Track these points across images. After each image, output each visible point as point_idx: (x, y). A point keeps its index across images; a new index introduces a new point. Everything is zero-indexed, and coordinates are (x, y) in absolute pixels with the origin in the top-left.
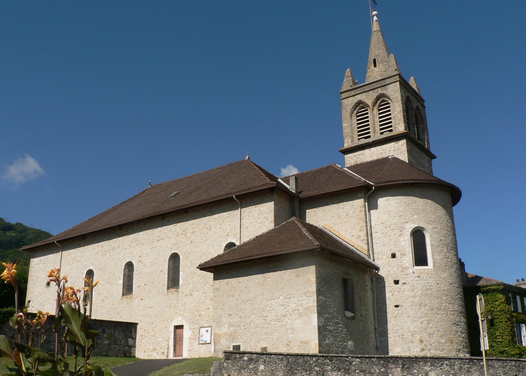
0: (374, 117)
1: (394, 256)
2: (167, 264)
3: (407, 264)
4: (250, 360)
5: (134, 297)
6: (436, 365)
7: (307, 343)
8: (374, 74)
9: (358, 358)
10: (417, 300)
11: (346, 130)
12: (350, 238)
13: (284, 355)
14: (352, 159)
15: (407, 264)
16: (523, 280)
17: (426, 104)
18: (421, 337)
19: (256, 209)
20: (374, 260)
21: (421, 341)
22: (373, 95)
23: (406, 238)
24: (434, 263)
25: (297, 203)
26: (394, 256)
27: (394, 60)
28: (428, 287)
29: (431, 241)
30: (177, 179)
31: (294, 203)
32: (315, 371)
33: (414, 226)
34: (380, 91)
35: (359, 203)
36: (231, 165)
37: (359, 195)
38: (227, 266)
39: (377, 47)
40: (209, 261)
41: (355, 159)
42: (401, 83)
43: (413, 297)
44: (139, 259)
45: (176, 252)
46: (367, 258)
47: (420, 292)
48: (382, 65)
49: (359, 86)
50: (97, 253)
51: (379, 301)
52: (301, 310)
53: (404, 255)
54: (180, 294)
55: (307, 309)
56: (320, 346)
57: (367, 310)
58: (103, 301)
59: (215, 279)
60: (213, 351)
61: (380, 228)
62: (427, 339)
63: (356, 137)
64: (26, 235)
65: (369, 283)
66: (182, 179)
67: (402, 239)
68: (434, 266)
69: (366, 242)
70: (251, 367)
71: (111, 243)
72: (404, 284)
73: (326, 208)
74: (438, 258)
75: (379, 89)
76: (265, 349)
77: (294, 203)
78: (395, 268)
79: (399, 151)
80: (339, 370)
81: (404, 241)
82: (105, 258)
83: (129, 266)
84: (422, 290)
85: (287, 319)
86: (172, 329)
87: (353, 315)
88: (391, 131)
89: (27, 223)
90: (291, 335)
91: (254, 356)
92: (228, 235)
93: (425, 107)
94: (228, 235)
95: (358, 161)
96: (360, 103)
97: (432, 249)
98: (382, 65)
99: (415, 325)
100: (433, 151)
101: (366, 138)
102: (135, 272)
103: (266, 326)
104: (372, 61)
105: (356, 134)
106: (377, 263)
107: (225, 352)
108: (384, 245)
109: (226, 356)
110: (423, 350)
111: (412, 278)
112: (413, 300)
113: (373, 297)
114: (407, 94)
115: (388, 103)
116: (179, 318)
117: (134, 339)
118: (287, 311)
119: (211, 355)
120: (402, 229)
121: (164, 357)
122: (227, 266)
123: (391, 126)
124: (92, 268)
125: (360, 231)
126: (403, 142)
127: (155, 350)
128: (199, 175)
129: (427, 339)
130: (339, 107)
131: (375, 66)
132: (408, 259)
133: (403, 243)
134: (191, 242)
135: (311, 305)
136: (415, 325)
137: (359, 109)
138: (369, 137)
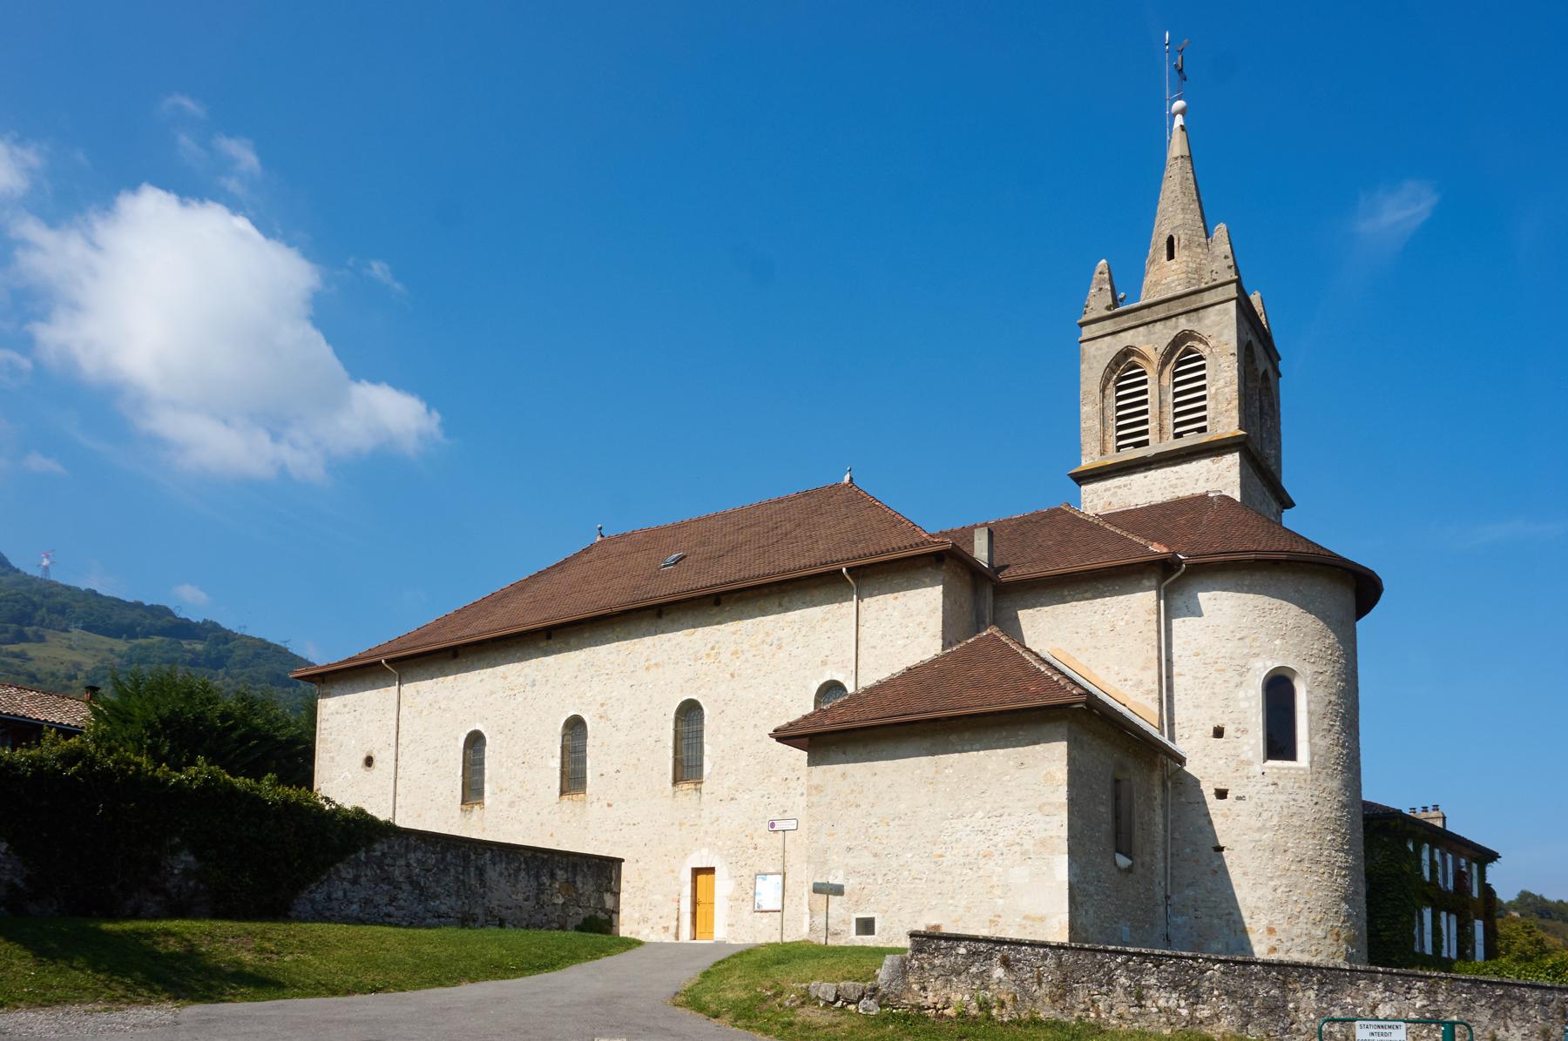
0: (1158, 388)
1: (1219, 733)
2: (671, 725)
3: (1250, 754)
4: (973, 954)
5: (589, 799)
6: (1397, 989)
7: (1042, 919)
8: (1165, 277)
9: (1220, 961)
10: (1267, 837)
11: (1089, 423)
12: (1118, 686)
13: (1051, 947)
14: (1098, 499)
15: (1250, 754)
16: (1436, 808)
17: (1282, 366)
18: (1271, 922)
19: (897, 603)
20: (1172, 738)
21: (1271, 931)
22: (1163, 335)
23: (1252, 692)
24: (1312, 754)
25: (989, 592)
26: (1219, 733)
27: (1226, 239)
28: (1294, 809)
29: (1309, 703)
30: (670, 523)
31: (985, 591)
32: (1121, 986)
33: (1272, 665)
34: (1183, 324)
35: (1143, 602)
36: (806, 494)
37: (1146, 583)
38: (837, 732)
39: (1174, 208)
40: (797, 722)
41: (1107, 496)
42: (1239, 305)
43: (1259, 830)
44: (601, 710)
45: (694, 697)
46: (1155, 733)
47: (1275, 820)
48: (1185, 259)
49: (1120, 310)
50: (492, 693)
51: (1177, 835)
52: (1028, 844)
53: (1245, 731)
54: (705, 797)
55: (1043, 843)
56: (1072, 928)
57: (1153, 854)
58: (512, 804)
59: (811, 762)
60: (806, 929)
61: (1196, 669)
62: (1285, 926)
63: (1112, 443)
64: (231, 651)
65: (1158, 792)
66: (682, 525)
67: (1241, 694)
68: (1311, 762)
69: (1156, 695)
70: (973, 970)
71: (527, 670)
72: (1239, 798)
73: (1098, 602)
74: (1323, 743)
75: (1182, 320)
76: (937, 927)
77: (985, 591)
78: (1221, 762)
79: (1221, 477)
80: (1175, 988)
81: (1247, 699)
82: (518, 701)
83: (575, 726)
84: (1280, 815)
85: (991, 863)
86: (687, 876)
87: (1129, 862)
88: (1203, 430)
89: (229, 622)
90: (1001, 902)
91: (982, 947)
92: (824, 663)
93: (1279, 375)
94: (824, 663)
95: (1114, 500)
96: (1127, 352)
97: (1310, 721)
98: (1185, 259)
99: (1259, 893)
100: (1288, 483)
101: (1137, 445)
102: (589, 741)
103: (939, 877)
104: (1164, 240)
105: (1112, 434)
106: (1180, 746)
107: (913, 935)
108: (1197, 707)
109: (915, 943)
110: (1274, 950)
111: (1258, 787)
112: (1257, 836)
113: (1165, 826)
114: (1250, 337)
115: (1201, 358)
116: (705, 851)
117: (617, 894)
118: (991, 847)
119: (805, 937)
120: (1243, 670)
121: (669, 938)
122: (837, 732)
123: (1204, 418)
124: (479, 727)
125: (1144, 669)
126: (1232, 460)
127: (645, 920)
128: (725, 516)
129: (1285, 926)
130: (1074, 360)
131: (1171, 256)
132: (1252, 742)
133: (1244, 705)
134: (732, 675)
135: (1053, 833)
136: (1259, 893)
137: (1179, 364)
138: (1146, 443)
